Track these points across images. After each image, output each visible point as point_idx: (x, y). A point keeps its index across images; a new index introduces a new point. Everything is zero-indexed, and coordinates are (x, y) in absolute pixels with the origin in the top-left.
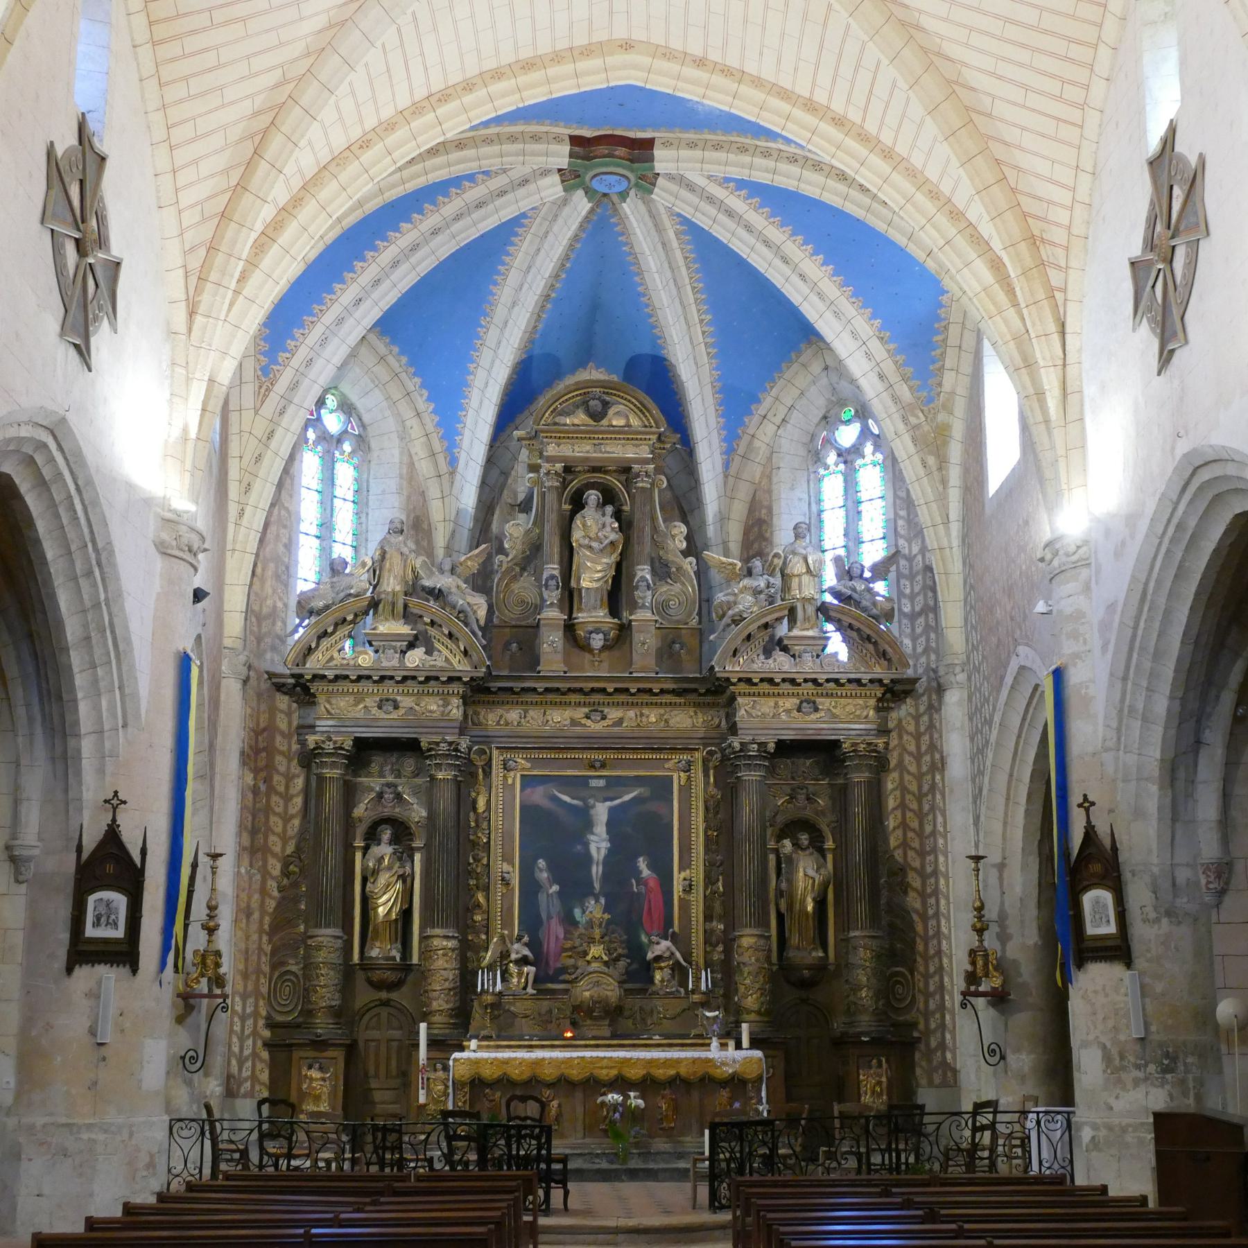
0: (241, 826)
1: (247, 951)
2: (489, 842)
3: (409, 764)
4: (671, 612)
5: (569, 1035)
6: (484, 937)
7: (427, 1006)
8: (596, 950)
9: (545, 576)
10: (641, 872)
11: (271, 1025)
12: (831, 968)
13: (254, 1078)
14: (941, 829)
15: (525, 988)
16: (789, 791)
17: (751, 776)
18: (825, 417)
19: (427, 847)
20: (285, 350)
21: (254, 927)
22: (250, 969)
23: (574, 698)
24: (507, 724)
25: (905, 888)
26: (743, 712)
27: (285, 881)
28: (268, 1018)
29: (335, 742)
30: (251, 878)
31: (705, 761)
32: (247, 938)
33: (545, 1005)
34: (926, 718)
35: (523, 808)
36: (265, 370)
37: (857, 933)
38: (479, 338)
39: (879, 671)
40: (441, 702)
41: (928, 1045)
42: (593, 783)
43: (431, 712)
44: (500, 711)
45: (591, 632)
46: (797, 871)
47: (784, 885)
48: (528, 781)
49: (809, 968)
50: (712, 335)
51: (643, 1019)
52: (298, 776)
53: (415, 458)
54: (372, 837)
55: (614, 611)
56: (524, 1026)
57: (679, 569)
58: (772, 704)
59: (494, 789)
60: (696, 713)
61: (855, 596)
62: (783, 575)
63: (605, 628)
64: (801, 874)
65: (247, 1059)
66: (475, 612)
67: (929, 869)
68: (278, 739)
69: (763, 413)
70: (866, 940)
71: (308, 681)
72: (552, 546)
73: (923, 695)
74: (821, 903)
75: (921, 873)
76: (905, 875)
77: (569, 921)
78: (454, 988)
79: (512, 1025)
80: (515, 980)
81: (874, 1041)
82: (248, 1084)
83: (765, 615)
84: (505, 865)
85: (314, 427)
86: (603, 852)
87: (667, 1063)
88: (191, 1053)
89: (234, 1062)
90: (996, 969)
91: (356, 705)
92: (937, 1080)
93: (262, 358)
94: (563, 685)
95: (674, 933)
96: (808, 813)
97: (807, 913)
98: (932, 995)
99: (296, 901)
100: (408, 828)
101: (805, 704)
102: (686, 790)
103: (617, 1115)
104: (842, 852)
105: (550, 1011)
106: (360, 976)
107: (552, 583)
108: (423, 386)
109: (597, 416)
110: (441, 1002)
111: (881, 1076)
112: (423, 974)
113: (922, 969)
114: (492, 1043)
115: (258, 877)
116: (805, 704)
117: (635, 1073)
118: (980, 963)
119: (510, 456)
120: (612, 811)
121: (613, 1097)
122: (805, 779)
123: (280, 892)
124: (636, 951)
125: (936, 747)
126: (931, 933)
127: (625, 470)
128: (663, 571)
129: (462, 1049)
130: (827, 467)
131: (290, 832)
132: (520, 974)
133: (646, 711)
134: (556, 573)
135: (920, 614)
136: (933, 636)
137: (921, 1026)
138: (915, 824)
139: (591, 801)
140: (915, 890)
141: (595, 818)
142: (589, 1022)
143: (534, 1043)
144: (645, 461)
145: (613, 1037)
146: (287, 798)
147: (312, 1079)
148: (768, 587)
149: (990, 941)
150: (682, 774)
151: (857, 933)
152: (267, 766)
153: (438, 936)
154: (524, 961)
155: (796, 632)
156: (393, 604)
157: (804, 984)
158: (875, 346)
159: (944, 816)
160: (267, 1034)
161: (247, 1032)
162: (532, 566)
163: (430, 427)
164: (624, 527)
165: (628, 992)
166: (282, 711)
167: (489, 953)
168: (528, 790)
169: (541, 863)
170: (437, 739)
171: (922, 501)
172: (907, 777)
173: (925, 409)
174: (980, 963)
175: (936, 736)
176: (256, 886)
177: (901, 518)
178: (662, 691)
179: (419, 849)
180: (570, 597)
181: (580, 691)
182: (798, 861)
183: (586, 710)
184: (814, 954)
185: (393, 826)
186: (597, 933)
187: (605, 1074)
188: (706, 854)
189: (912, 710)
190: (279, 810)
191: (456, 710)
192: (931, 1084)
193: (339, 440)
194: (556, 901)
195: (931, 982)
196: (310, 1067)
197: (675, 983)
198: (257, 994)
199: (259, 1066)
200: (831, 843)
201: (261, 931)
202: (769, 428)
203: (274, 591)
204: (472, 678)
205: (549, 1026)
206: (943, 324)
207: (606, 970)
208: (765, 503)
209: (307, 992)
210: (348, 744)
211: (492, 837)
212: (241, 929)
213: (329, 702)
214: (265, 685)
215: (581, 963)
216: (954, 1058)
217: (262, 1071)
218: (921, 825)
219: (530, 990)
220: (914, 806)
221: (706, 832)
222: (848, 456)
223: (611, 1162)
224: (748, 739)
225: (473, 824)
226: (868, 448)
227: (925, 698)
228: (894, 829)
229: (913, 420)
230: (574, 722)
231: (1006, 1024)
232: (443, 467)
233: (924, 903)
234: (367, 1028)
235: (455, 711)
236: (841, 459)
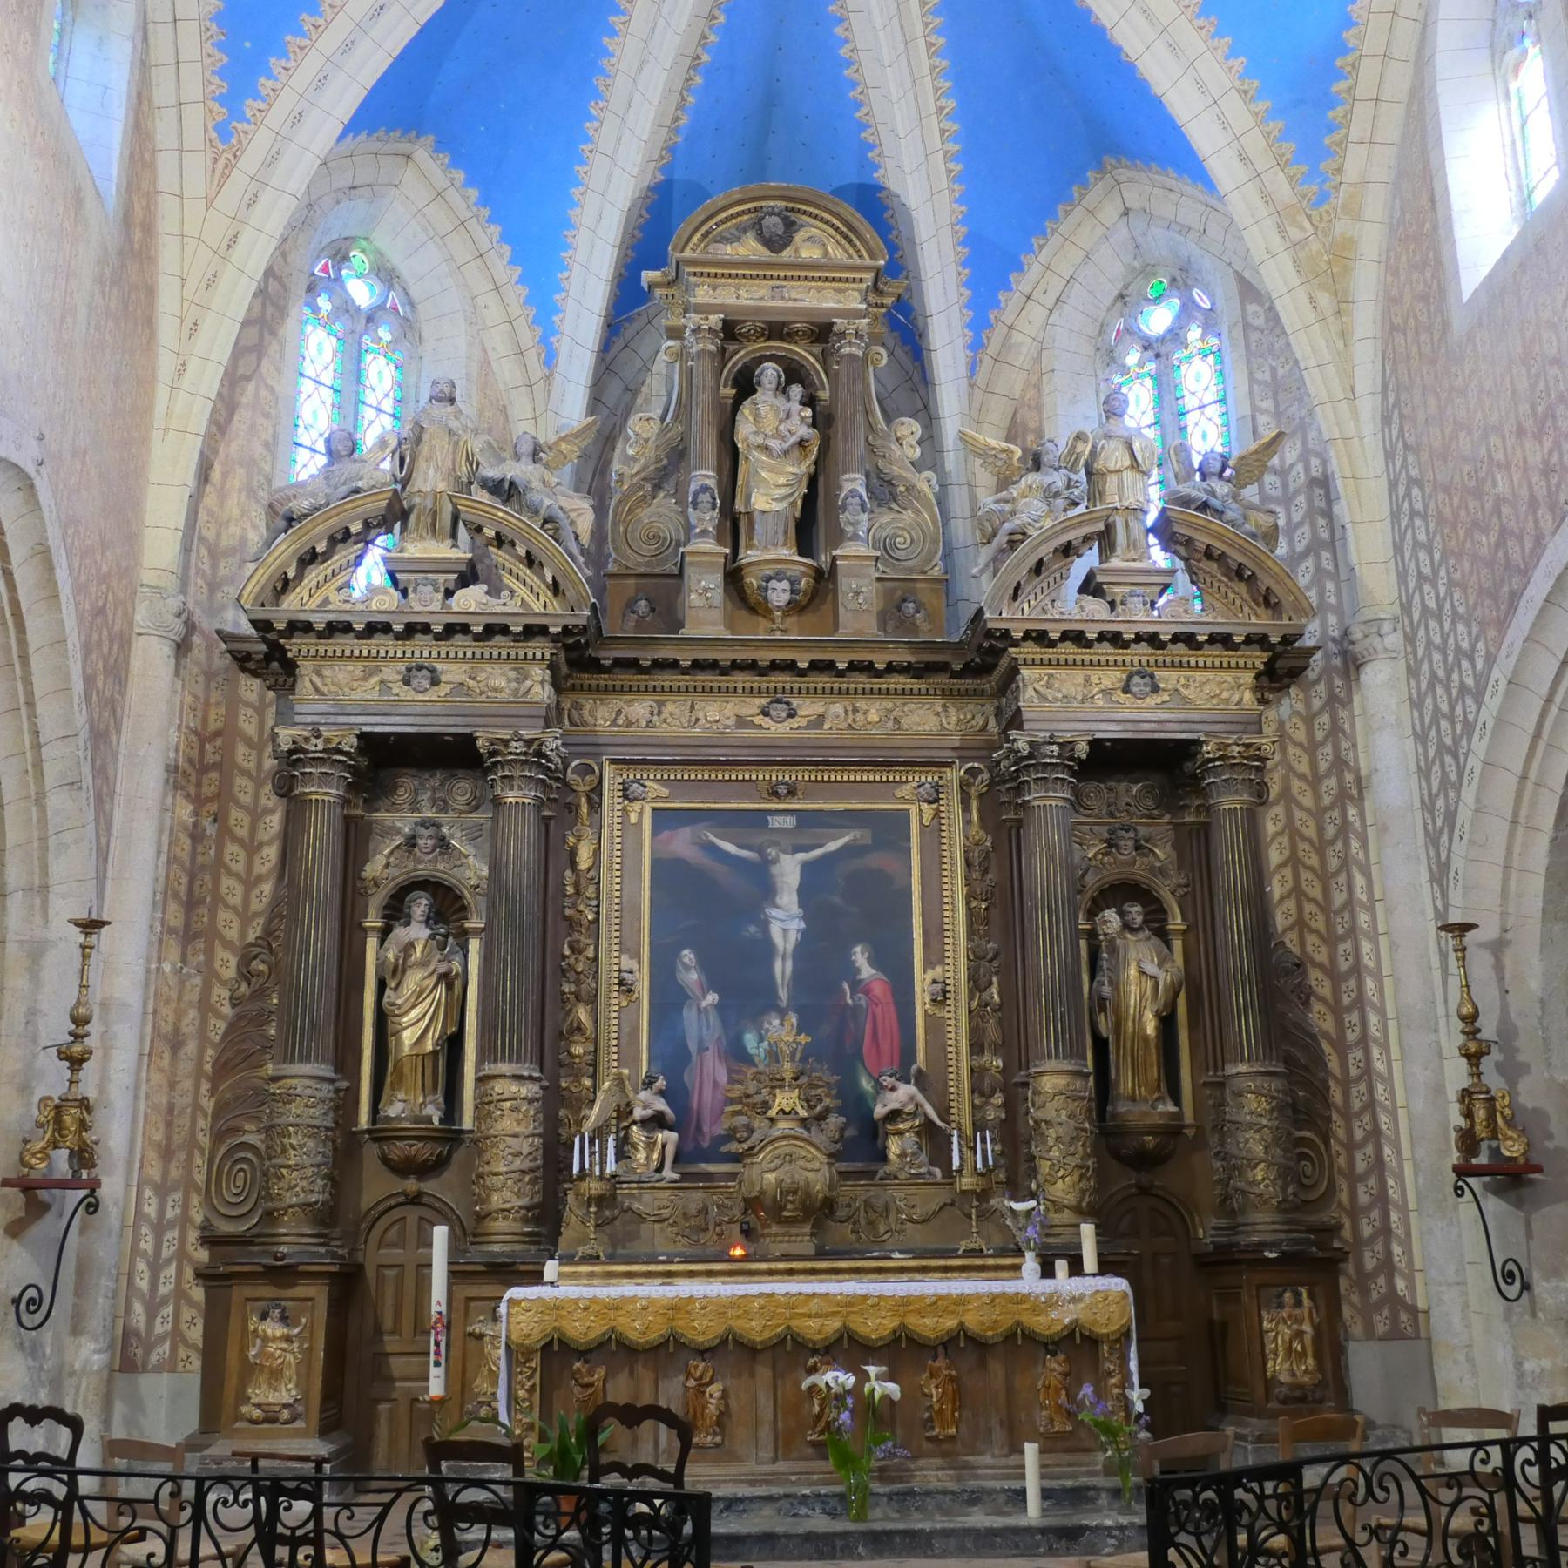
0: (167, 893)
1: (171, 1109)
2: (597, 921)
3: (462, 789)
4: (899, 554)
5: (738, 1252)
6: (588, 1082)
7: (486, 1201)
8: (785, 1099)
9: (692, 488)
10: (858, 971)
11: (210, 1240)
12: (1190, 1132)
13: (177, 1336)
14: (1364, 898)
15: (659, 1169)
16: (1106, 835)
17: (1048, 799)
18: (1121, 296)
19: (486, 932)
20: (257, 96)
21: (186, 1067)
22: (177, 1139)
23: (741, 679)
24: (629, 724)
25: (1305, 996)
26: (1030, 692)
27: (244, 988)
28: (206, 1227)
29: (328, 741)
30: (182, 983)
31: (964, 787)
32: (172, 1085)
33: (695, 1199)
34: (1325, 719)
35: (656, 863)
36: (224, 132)
37: (1242, 1068)
38: (588, 140)
39: (1260, 621)
40: (513, 674)
41: (1359, 1266)
42: (775, 822)
43: (496, 690)
44: (616, 702)
45: (768, 579)
46: (1126, 965)
47: (1106, 990)
48: (664, 819)
49: (1152, 1131)
50: (955, 138)
51: (872, 1224)
52: (272, 811)
53: (492, 355)
54: (396, 912)
55: (805, 545)
56: (658, 1238)
57: (910, 488)
58: (1081, 680)
59: (605, 832)
60: (945, 707)
61: (1214, 502)
62: (1089, 473)
63: (794, 571)
64: (1133, 972)
65: (164, 1302)
66: (572, 523)
67: (1344, 966)
68: (241, 749)
69: (1027, 290)
70: (1259, 1081)
71: (281, 634)
72: (706, 443)
73: (1317, 681)
74: (1167, 1022)
75: (1332, 972)
76: (1305, 974)
77: (737, 1055)
78: (532, 1170)
79: (633, 1236)
80: (641, 1156)
81: (1287, 1259)
82: (166, 1347)
83: (1066, 530)
84: (625, 958)
85: (330, 292)
86: (793, 937)
87: (938, 1305)
88: (32, 1293)
89: (138, 1307)
90: (1510, 1123)
91: (365, 679)
92: (1381, 1328)
93: (216, 107)
94: (724, 656)
95: (919, 1071)
96: (1139, 870)
97: (1146, 1039)
98: (1363, 1178)
99: (261, 1019)
100: (459, 898)
101: (1136, 679)
102: (933, 832)
103: (845, 1417)
104: (1204, 927)
105: (704, 1211)
106: (371, 1152)
107: (706, 497)
108: (504, 238)
109: (775, 244)
110: (506, 1194)
111: (1301, 1322)
112: (479, 1143)
113: (1341, 1133)
114: (597, 1269)
115: (198, 980)
116: (1136, 679)
117: (875, 1327)
118: (1480, 1113)
119: (639, 364)
120: (806, 867)
121: (836, 1378)
122: (1132, 815)
123: (234, 1006)
124: (856, 1107)
125: (1347, 764)
126: (1354, 1072)
127: (822, 333)
128: (884, 491)
129: (536, 1277)
130: (1125, 370)
131: (256, 905)
132: (650, 1145)
133: (861, 704)
134: (712, 483)
135: (1305, 555)
136: (1330, 586)
137: (1347, 1233)
138: (1316, 892)
139: (772, 852)
140: (1322, 999)
141: (778, 880)
142: (774, 1229)
143: (673, 1268)
144: (858, 314)
145: (821, 1255)
146: (252, 848)
147: (266, 1339)
148: (1068, 487)
149: (1494, 1081)
150: (925, 806)
151: (1242, 1068)
152: (218, 796)
153: (503, 1076)
154: (656, 1122)
155: (1115, 563)
156: (434, 515)
157: (1144, 1161)
158: (1235, 107)
159: (1368, 876)
160: (203, 1255)
161: (166, 1253)
162: (672, 481)
163: (516, 309)
164: (820, 419)
165: (844, 1175)
166: (248, 705)
167: (597, 1108)
168: (665, 834)
169: (688, 956)
170: (505, 734)
171: (1312, 363)
172: (1298, 814)
173: (1314, 213)
174: (1480, 1113)
175: (1344, 744)
176: (194, 996)
177: (1263, 412)
178: (891, 669)
179: (477, 932)
180: (733, 525)
181: (752, 666)
182: (1126, 947)
183: (763, 701)
184: (1161, 1108)
185: (434, 896)
186: (788, 1069)
187: (817, 1329)
188: (969, 939)
189: (1300, 707)
190: (239, 867)
191: (538, 687)
192: (1370, 1334)
193: (371, 318)
194: (713, 1018)
195: (1359, 1156)
196: (264, 1316)
197: (923, 1158)
198: (188, 1185)
199: (187, 1313)
200: (1179, 921)
201: (199, 1074)
202: (1036, 313)
203: (244, 513)
204: (565, 628)
205: (704, 1238)
206: (1350, 59)
207: (805, 1133)
208: (1032, 425)
209: (265, 1177)
210: (350, 743)
211: (603, 911)
212: (161, 1070)
213: (319, 674)
214: (223, 662)
215: (759, 1123)
216: (1412, 1286)
217: (192, 1322)
218: (1326, 891)
219: (668, 1173)
220: (1313, 861)
221: (968, 903)
222: (1158, 349)
223: (833, 1514)
224: (1042, 736)
225: (570, 890)
226: (1194, 333)
227: (1322, 687)
228: (1282, 898)
229: (1294, 233)
230: (741, 722)
231: (1528, 1225)
232: (536, 370)
233: (1339, 1022)
234: (379, 1247)
235: (537, 688)
236: (1150, 354)
